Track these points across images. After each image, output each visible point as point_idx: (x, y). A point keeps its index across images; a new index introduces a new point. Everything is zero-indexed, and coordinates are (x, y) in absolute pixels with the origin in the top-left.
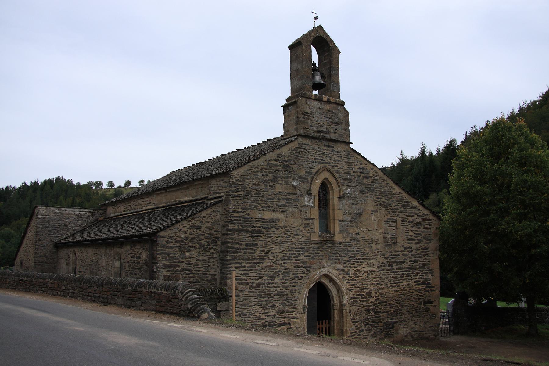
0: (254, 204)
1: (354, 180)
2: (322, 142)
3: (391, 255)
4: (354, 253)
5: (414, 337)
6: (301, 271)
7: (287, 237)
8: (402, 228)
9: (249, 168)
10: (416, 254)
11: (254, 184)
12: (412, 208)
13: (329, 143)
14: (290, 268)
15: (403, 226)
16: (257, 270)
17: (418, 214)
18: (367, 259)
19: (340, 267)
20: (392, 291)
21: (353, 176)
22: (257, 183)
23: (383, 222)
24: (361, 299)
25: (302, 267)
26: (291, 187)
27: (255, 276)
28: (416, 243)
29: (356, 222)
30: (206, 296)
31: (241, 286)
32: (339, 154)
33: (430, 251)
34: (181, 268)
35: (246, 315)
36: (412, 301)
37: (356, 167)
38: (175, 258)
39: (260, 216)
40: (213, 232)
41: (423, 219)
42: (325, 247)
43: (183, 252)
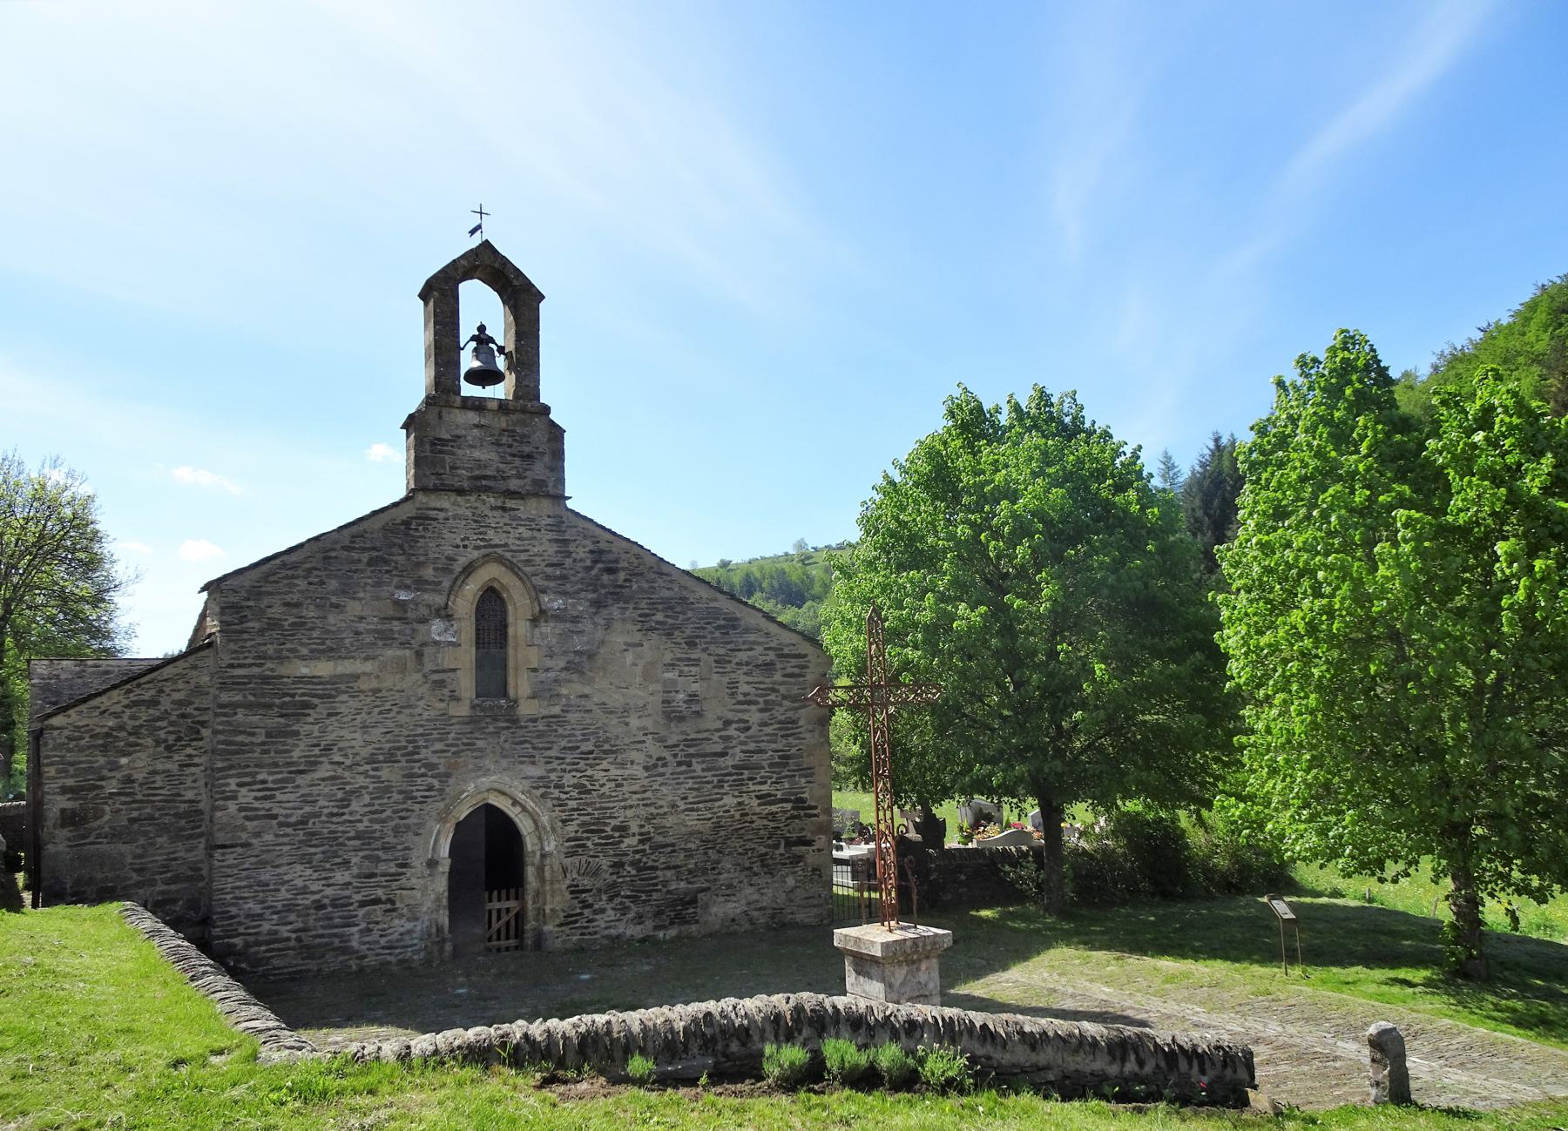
7: (380, 713)
8: (715, 677)
25: (423, 775)
28: (761, 710)
29: (582, 673)
31: (255, 823)
35: (268, 885)
37: (581, 550)
40: (190, 710)
42: (491, 729)
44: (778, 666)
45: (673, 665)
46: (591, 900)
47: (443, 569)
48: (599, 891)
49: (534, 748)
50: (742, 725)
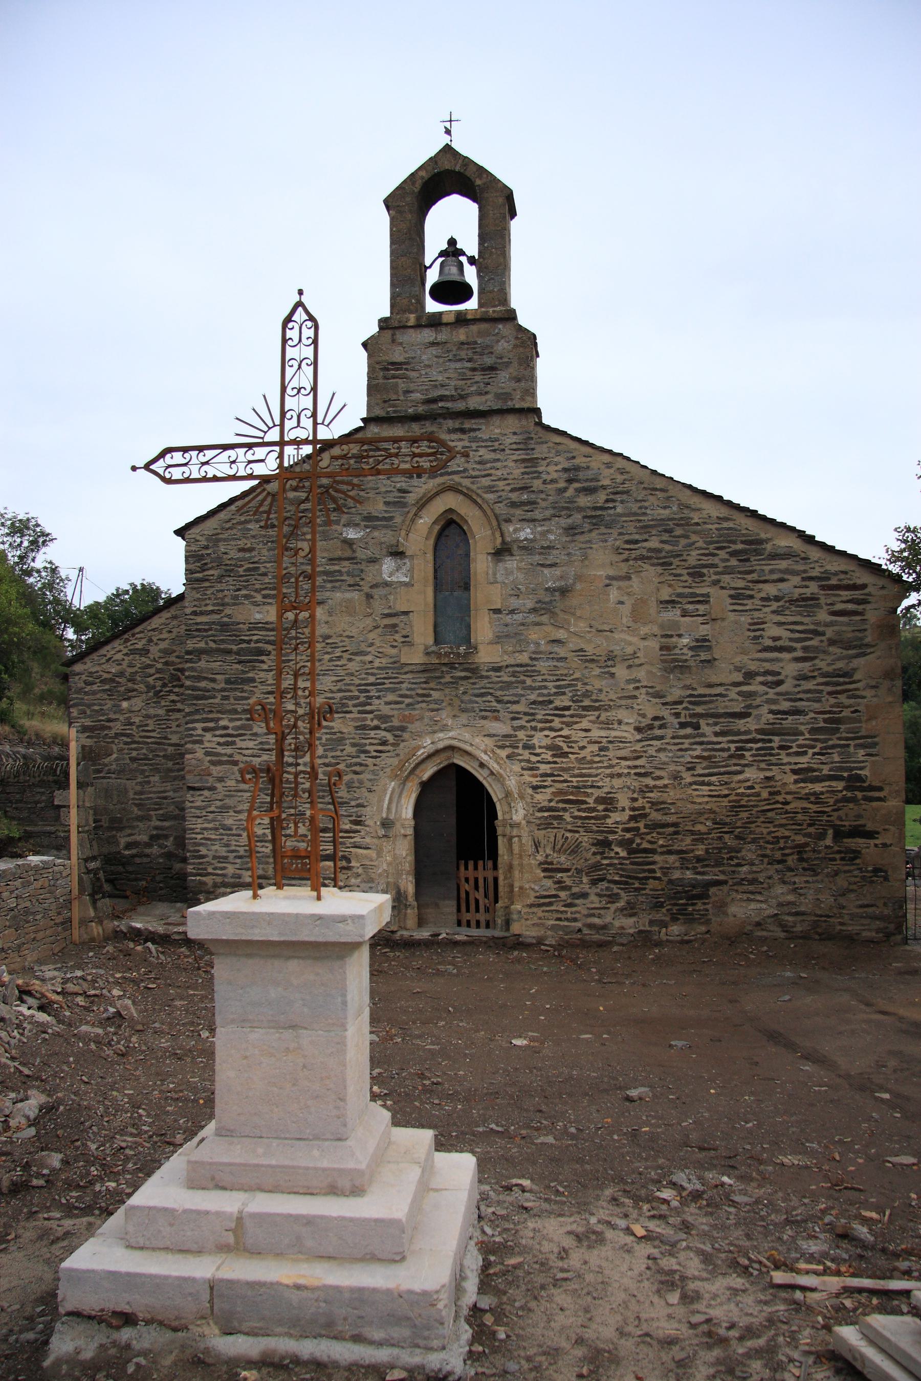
0: (244, 592)
2: (440, 424)
5: (795, 929)
6: (375, 738)
7: (331, 660)
8: (732, 616)
10: (796, 690)
11: (242, 550)
12: (774, 556)
13: (462, 423)
14: (345, 730)
15: (735, 611)
16: (255, 734)
17: (805, 571)
19: (501, 728)
21: (542, 492)
22: (249, 545)
24: (577, 813)
25: (377, 728)
28: (797, 660)
29: (553, 614)
30: (34, 777)
31: (219, 768)
32: (496, 444)
33: (859, 681)
34: (113, 732)
35: (231, 829)
36: (781, 826)
37: (551, 469)
38: (101, 712)
39: (258, 616)
40: (172, 658)
41: (823, 588)
42: (448, 679)
43: (116, 702)
45: (673, 602)
46: (568, 882)
47: (395, 504)
48: (579, 871)
49: (499, 702)
50: (770, 678)
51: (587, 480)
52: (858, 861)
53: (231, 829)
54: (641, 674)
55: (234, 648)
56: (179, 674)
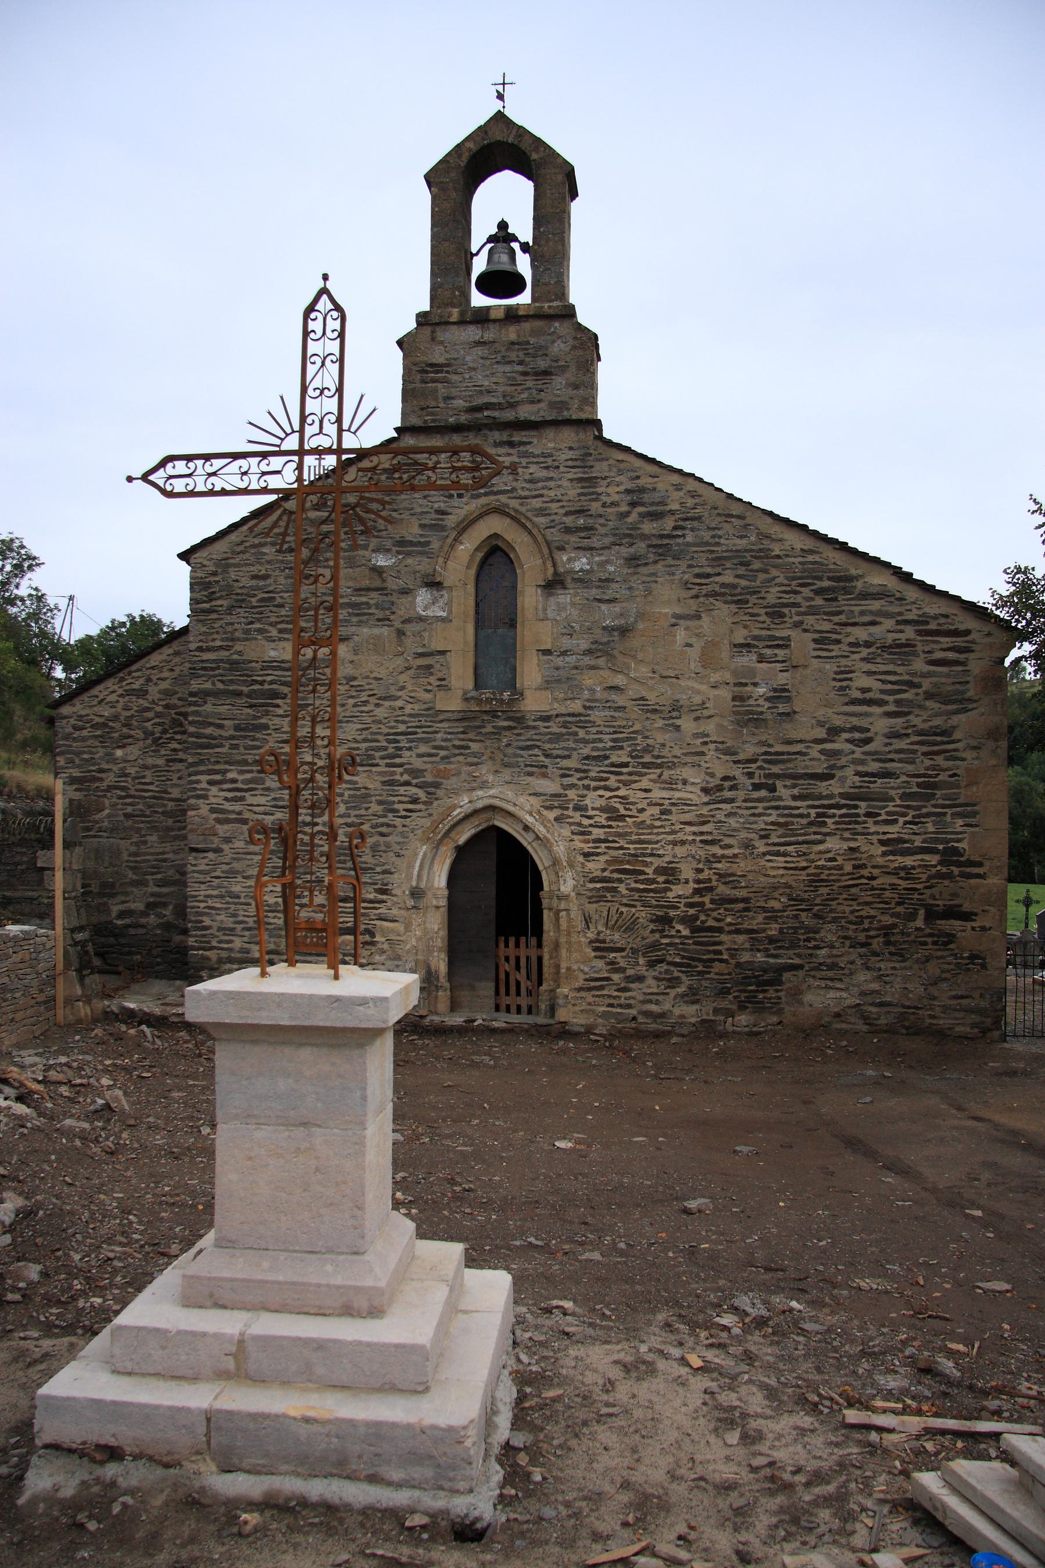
0: (258, 626)
1: (602, 530)
2: (485, 436)
3: (766, 753)
4: (600, 745)
7: (355, 705)
9: (239, 539)
10: (887, 749)
11: (255, 577)
12: (865, 596)
13: (511, 436)
14: (370, 786)
17: (900, 614)
18: (659, 766)
19: (550, 786)
20: (772, 868)
21: (601, 516)
22: (263, 572)
23: (726, 646)
24: (633, 885)
25: (407, 783)
26: (367, 571)
27: (262, 803)
28: (889, 715)
29: (611, 656)
30: (14, 834)
31: (226, 827)
32: (549, 460)
33: (959, 741)
35: (239, 897)
37: (612, 490)
39: (273, 653)
40: (174, 701)
42: (489, 729)
44: (920, 648)
45: (748, 645)
46: (623, 963)
48: (635, 951)
50: (857, 735)
51: (652, 504)
52: (952, 946)
53: (239, 897)
54: (710, 727)
55: (245, 689)
56: (181, 718)
